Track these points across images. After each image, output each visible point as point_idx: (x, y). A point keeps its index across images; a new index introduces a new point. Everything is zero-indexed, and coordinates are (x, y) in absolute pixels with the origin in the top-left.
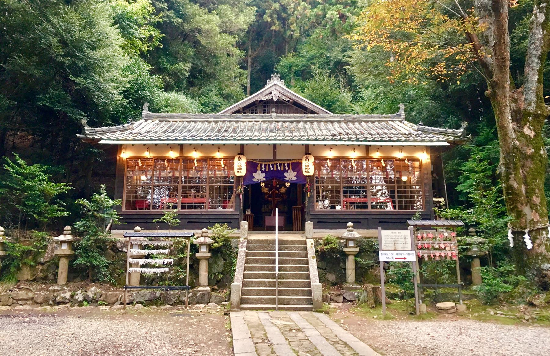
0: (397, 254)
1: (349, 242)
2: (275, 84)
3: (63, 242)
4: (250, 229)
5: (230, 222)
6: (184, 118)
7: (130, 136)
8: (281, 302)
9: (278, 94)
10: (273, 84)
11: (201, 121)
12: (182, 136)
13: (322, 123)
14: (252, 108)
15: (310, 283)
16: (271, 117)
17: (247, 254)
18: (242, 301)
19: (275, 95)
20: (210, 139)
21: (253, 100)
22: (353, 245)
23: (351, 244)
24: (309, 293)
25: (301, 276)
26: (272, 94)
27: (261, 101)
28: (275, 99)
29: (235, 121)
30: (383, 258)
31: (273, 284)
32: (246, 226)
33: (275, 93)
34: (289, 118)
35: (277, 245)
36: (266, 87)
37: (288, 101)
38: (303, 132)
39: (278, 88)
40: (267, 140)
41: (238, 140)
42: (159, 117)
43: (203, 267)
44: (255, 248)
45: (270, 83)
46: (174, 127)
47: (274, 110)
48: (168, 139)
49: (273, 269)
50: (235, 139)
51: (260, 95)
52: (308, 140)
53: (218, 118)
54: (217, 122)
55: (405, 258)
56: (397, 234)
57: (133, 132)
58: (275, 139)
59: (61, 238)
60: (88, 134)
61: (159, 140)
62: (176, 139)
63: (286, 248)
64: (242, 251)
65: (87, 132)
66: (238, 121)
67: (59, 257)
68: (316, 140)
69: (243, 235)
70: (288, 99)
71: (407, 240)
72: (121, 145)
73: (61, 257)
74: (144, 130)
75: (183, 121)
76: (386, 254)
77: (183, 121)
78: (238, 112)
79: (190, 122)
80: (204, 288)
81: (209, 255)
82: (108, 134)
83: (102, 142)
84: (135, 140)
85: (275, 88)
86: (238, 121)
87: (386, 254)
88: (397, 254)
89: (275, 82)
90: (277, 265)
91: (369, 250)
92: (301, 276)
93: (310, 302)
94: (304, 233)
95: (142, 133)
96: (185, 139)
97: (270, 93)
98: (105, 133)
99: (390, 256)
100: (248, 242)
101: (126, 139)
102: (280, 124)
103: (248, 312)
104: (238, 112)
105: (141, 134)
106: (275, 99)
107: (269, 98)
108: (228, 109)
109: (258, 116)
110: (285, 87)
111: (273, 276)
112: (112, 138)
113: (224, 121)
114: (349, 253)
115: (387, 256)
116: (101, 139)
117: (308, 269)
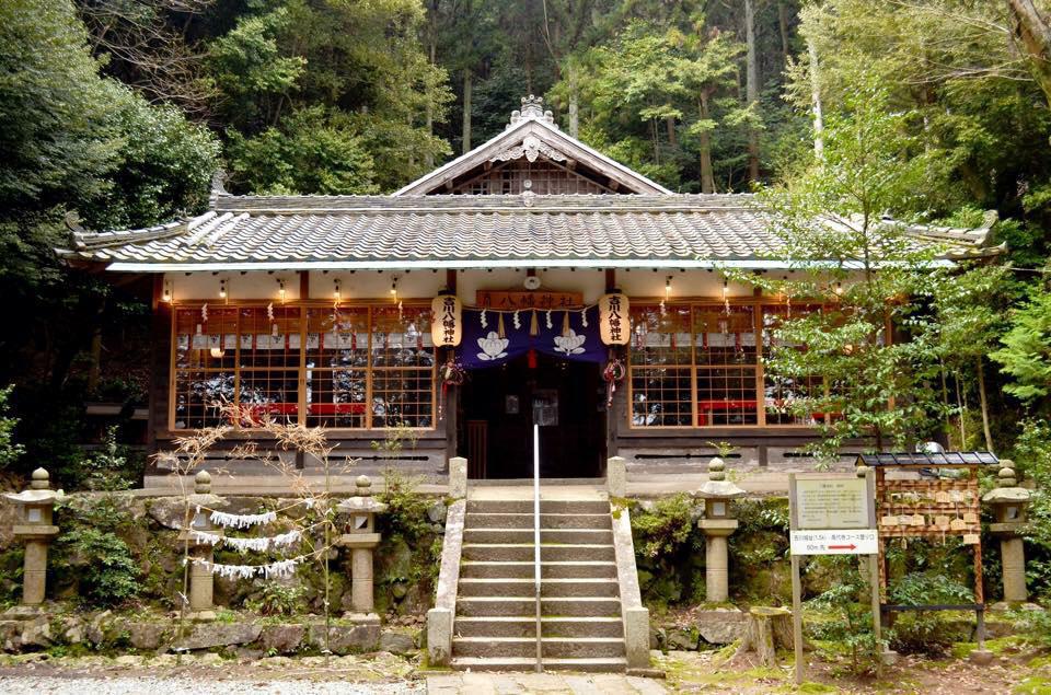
0: (834, 537)
1: (716, 505)
2: (532, 122)
3: (29, 506)
4: (472, 474)
5: (426, 458)
6: (310, 206)
7: (181, 252)
8: (549, 651)
9: (538, 145)
10: (526, 120)
11: (352, 214)
12: (305, 251)
13: (645, 216)
14: (473, 181)
15: (619, 605)
16: (522, 203)
17: (466, 538)
18: (456, 650)
19: (532, 148)
20: (372, 258)
21: (478, 161)
22: (724, 514)
23: (719, 510)
24: (617, 630)
25: (595, 571)
26: (526, 146)
27: (498, 162)
28: (532, 158)
29: (433, 213)
30: (799, 546)
31: (528, 609)
32: (464, 470)
33: (529, 142)
34: (566, 203)
35: (537, 515)
36: (509, 129)
37: (564, 163)
38: (600, 237)
39: (537, 130)
40: (512, 257)
41: (441, 259)
42: (251, 204)
43: (362, 568)
44: (485, 522)
45: (518, 119)
46: (287, 228)
47: (528, 184)
48: (271, 259)
49: (530, 572)
50: (433, 258)
51: (495, 149)
52: (612, 257)
53: (393, 206)
54: (389, 214)
55: (852, 547)
56: (835, 488)
57: (189, 243)
58: (532, 257)
59: (27, 496)
60: (82, 249)
61: (251, 260)
62: (291, 259)
63: (562, 521)
64: (455, 528)
65: (81, 244)
66: (441, 213)
67: (23, 542)
68: (633, 257)
69: (458, 494)
70: (564, 158)
71: (858, 503)
72: (160, 275)
73: (29, 541)
74: (214, 237)
75: (309, 215)
76: (806, 538)
77: (309, 215)
78: (442, 190)
79: (323, 215)
80: (363, 612)
81: (375, 538)
82: (129, 247)
83: (114, 267)
84: (191, 261)
85: (530, 131)
86: (441, 213)
87: (806, 538)
88: (834, 537)
89: (532, 116)
90: (538, 563)
91: (759, 530)
92: (595, 571)
93: (621, 650)
94: (603, 483)
95: (209, 243)
96: (311, 259)
97: (521, 144)
98: (118, 244)
99: (817, 543)
100: (469, 508)
101: (171, 260)
102: (544, 218)
103: (468, 676)
104: (442, 190)
105: (206, 247)
106: (532, 158)
107: (515, 155)
108: (614, 521)
109: (490, 200)
110: (555, 128)
111: (529, 590)
112: (138, 257)
113: (407, 214)
114: (714, 533)
115: (809, 542)
116: (113, 260)
117: (613, 572)
